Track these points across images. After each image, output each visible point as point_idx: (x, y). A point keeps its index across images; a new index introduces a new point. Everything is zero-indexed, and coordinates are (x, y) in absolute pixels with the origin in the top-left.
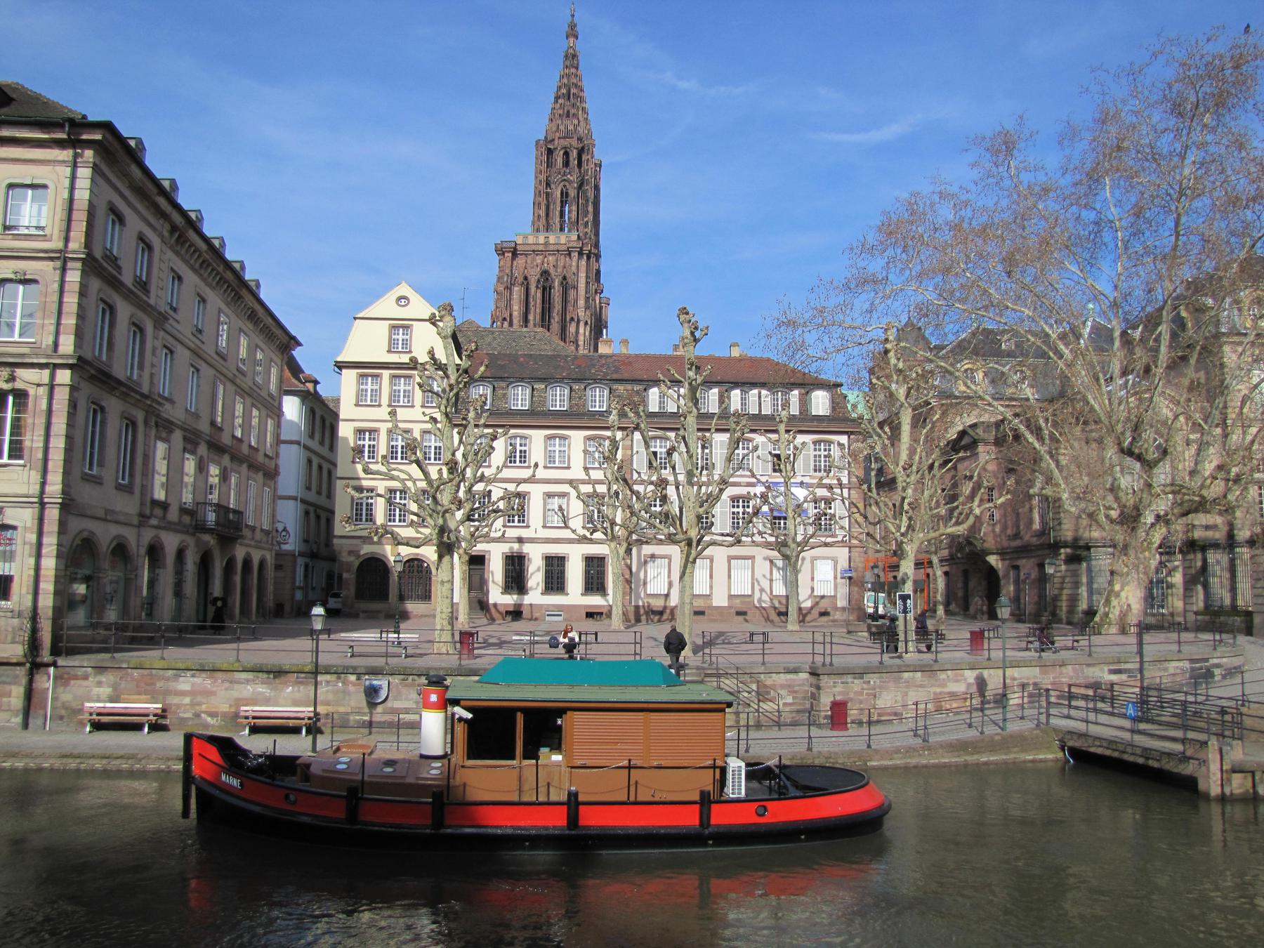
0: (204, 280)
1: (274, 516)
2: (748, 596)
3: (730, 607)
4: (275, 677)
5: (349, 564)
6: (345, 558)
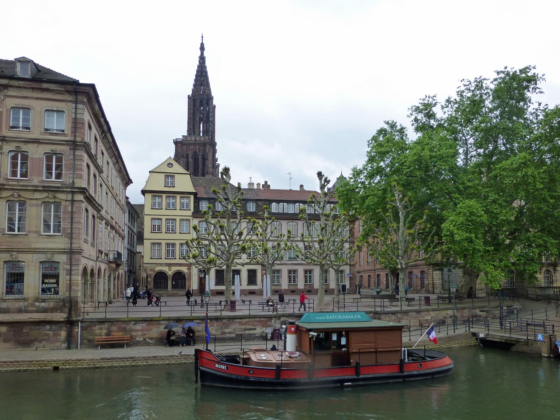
3: (305, 289)
4: (177, 322)
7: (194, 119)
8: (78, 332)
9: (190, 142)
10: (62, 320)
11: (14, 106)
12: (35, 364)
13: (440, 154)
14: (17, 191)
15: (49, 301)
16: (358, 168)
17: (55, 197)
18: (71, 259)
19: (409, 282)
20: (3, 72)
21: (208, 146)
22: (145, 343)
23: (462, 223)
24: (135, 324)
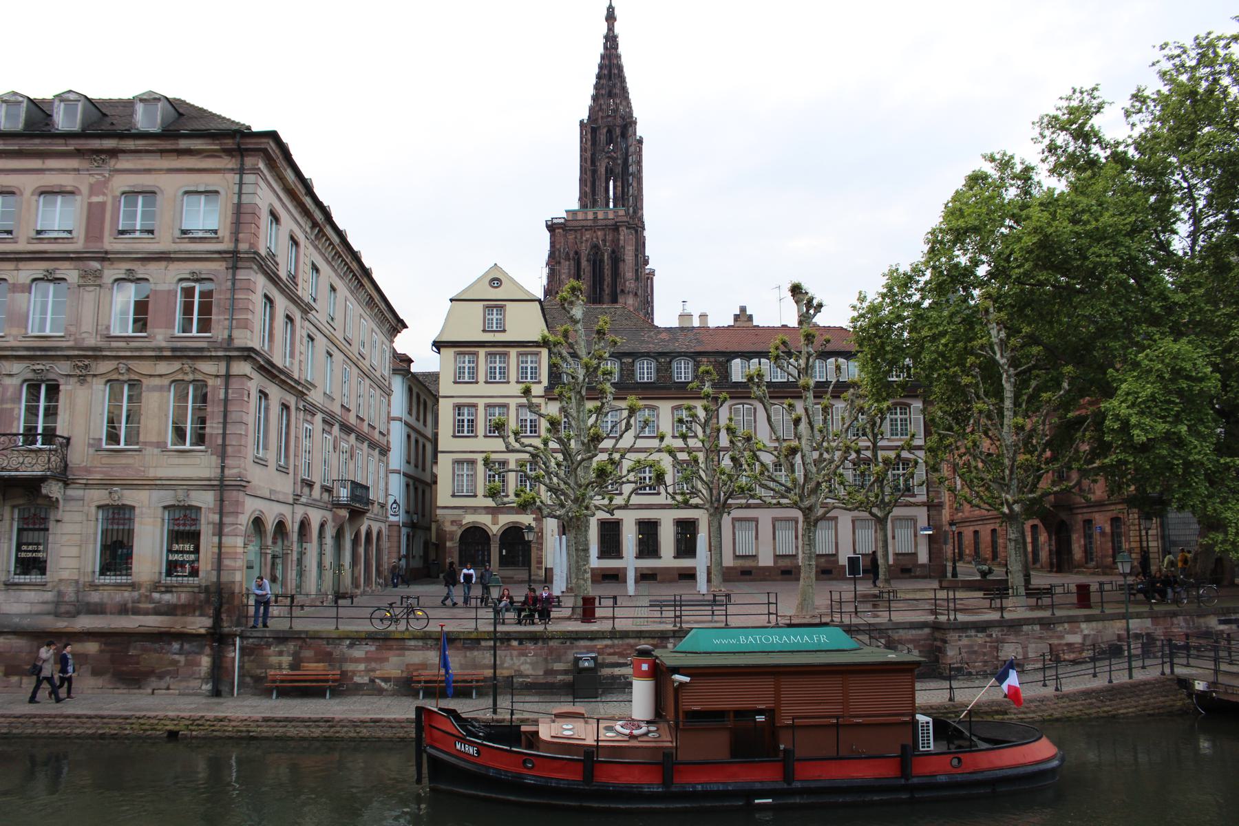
0: (335, 271)
1: (387, 489)
2: (793, 556)
5: (452, 533)
6: (448, 527)
7: (594, 172)
8: (234, 658)
9: (584, 223)
10: (203, 631)
11: (127, 189)
12: (132, 724)
13: (1097, 228)
14: (124, 361)
15: (179, 589)
16: (901, 271)
17: (195, 370)
18: (222, 501)
19: (1085, 545)
20: (112, 124)
21: (624, 231)
22: (373, 689)
23: (1153, 398)
24: (351, 646)
